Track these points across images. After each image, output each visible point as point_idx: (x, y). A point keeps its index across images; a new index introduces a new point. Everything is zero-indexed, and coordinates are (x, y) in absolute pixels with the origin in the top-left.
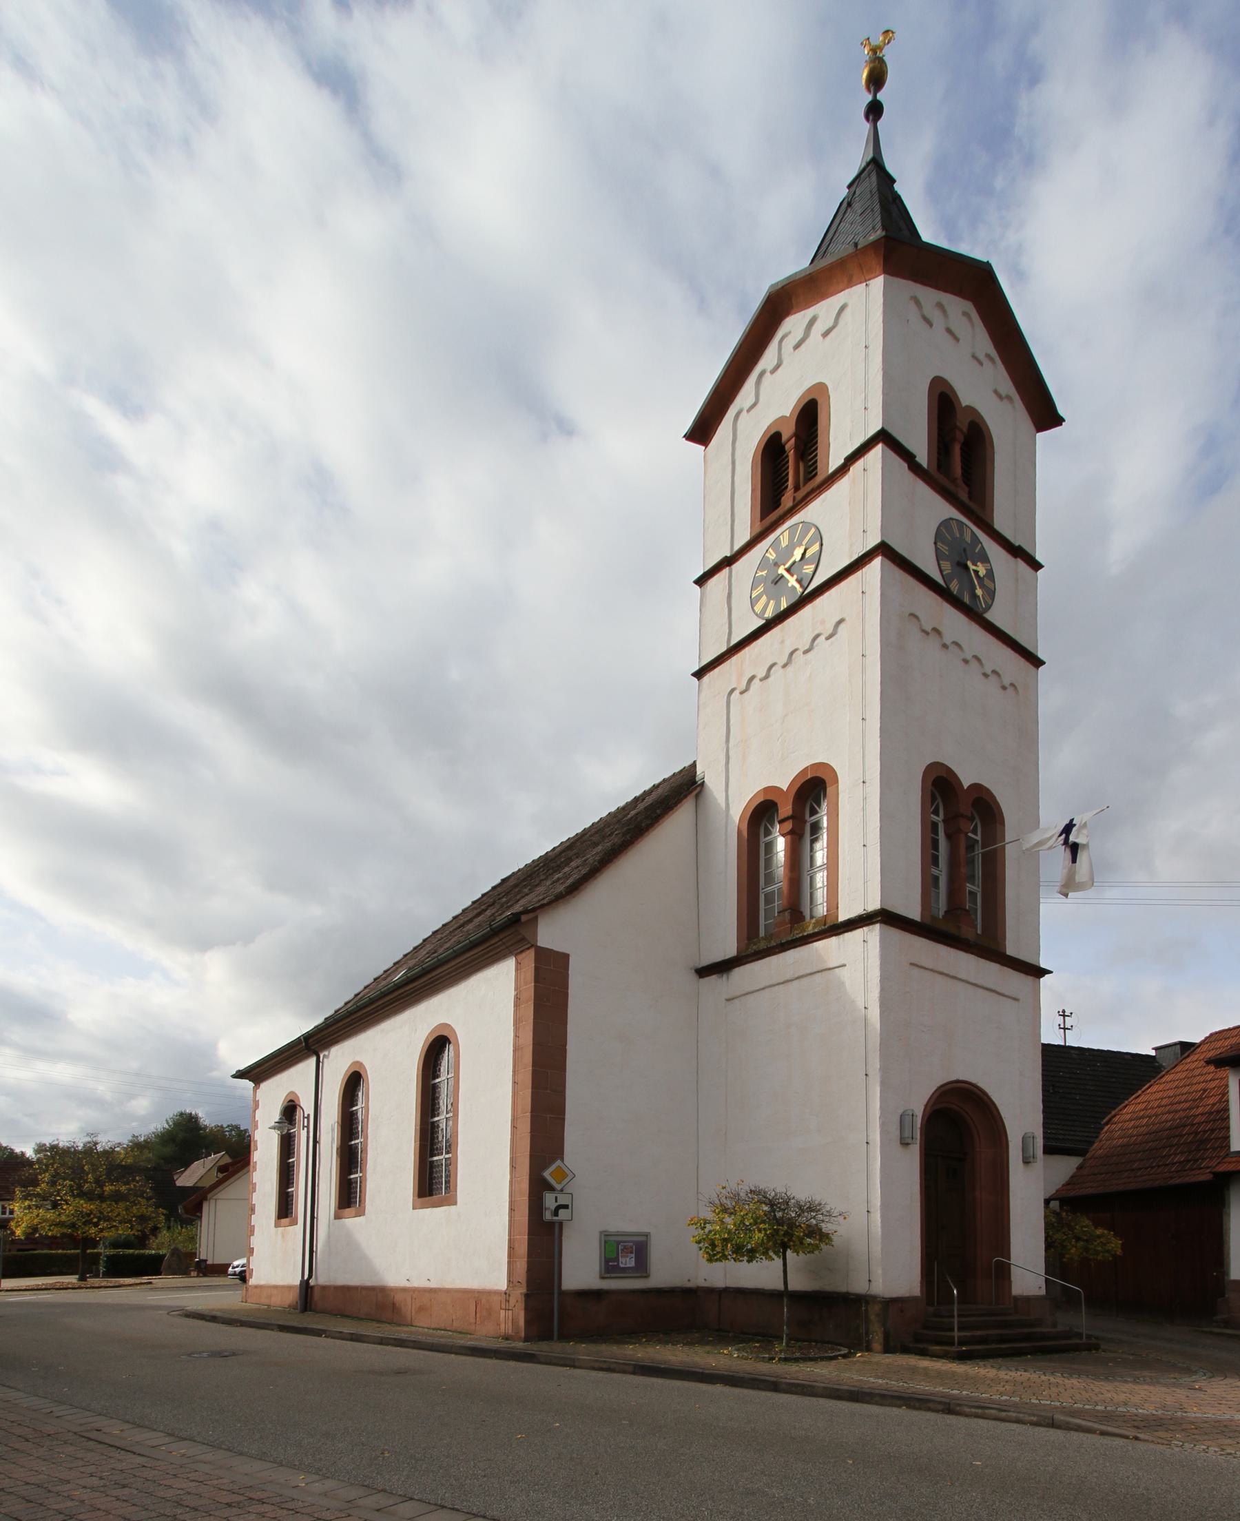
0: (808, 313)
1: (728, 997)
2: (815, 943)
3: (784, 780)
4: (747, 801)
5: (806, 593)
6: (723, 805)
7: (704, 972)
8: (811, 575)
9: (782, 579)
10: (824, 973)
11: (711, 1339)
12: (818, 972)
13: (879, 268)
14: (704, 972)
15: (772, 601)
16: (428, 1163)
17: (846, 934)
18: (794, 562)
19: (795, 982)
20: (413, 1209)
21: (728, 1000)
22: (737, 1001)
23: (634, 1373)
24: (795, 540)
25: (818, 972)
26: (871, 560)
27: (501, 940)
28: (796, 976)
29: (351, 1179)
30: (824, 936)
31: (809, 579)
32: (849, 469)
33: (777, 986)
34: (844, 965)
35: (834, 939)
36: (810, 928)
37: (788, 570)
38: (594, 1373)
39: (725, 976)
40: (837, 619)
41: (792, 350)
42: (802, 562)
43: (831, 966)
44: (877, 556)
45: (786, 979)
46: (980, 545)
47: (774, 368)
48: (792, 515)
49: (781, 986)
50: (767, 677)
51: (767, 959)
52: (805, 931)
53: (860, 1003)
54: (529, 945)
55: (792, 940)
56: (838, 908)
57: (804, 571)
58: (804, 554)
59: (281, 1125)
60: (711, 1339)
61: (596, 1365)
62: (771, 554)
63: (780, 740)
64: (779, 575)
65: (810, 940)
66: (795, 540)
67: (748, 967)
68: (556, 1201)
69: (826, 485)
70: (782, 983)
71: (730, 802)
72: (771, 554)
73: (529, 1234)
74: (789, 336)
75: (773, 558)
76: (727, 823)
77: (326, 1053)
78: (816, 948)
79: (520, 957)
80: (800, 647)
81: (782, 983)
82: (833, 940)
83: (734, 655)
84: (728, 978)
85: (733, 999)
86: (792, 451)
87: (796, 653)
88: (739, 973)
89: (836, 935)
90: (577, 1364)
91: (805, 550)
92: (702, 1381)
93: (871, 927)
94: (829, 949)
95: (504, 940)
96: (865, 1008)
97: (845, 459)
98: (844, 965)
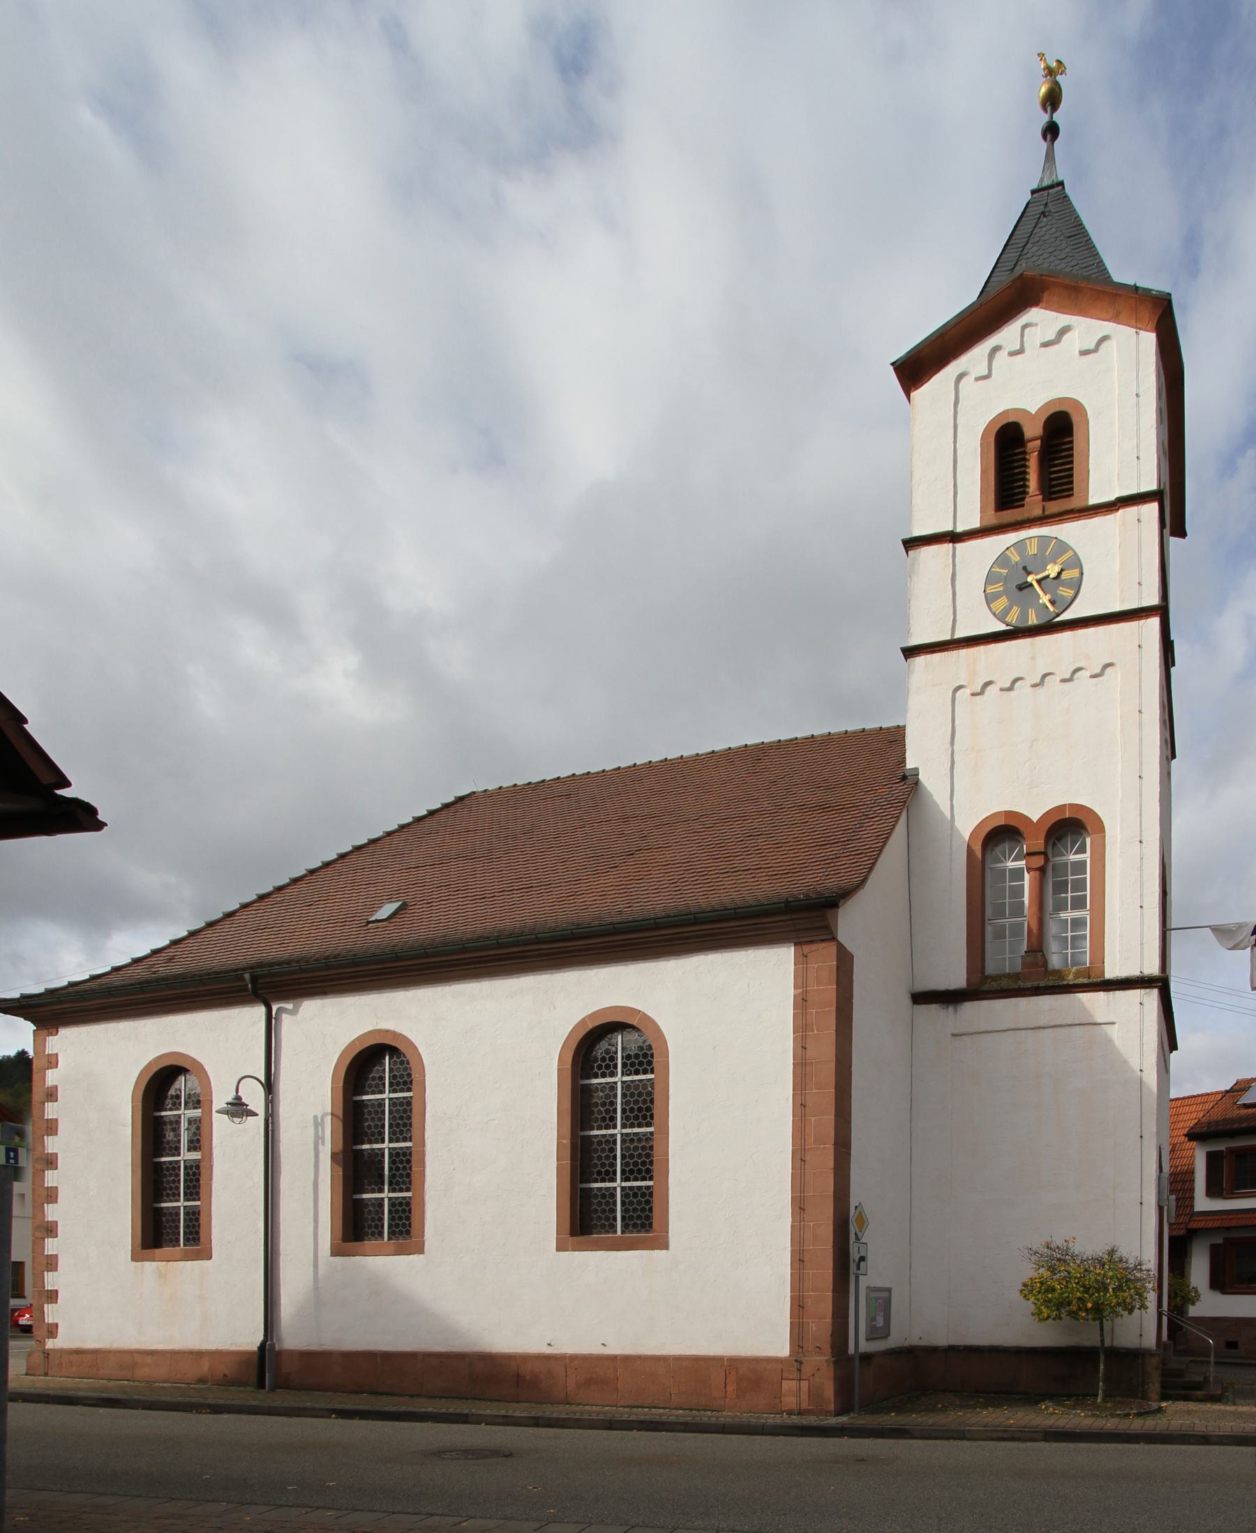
0: (1064, 319)
1: (955, 1032)
2: (1077, 994)
3: (1034, 810)
4: (981, 820)
5: (1058, 619)
6: (949, 816)
7: (920, 998)
8: (1070, 601)
9: (1030, 588)
10: (1086, 1027)
11: (961, 1414)
12: (1080, 1025)
13: (1153, 325)
14: (920, 998)
15: (1015, 608)
16: (579, 1190)
17: (1117, 992)
18: (1048, 576)
19: (1049, 1030)
20: (558, 1249)
21: (954, 1035)
22: (965, 1038)
23: (1046, 1440)
24: (1047, 553)
25: (1080, 1025)
26: (1147, 617)
27: (792, 920)
28: (1052, 1024)
29: (162, 1208)
30: (1091, 989)
31: (1067, 605)
32: (1118, 509)
33: (1024, 1031)
34: (1113, 1023)
35: (1101, 994)
36: (1071, 977)
37: (1039, 582)
38: (1003, 1444)
39: (951, 1009)
40: (1107, 661)
41: (1038, 345)
42: (1056, 581)
43: (1099, 1021)
44: (1155, 615)
45: (1039, 1025)
46: (993, 570)
47: (1015, 351)
48: (1042, 525)
49: (1030, 1032)
50: (1011, 689)
51: (1013, 1000)
52: (1064, 979)
53: (1135, 1063)
54: (830, 937)
55: (1052, 986)
56: (1104, 963)
57: (1058, 591)
58: (1059, 574)
59: (235, 1108)
60: (961, 1414)
61: (995, 1435)
62: (1012, 553)
63: (1027, 764)
64: (1027, 582)
65: (1074, 990)
66: (1047, 553)
67: (984, 1004)
68: (859, 1253)
69: (1093, 512)
70: (1032, 1029)
71: (955, 813)
72: (1012, 553)
73: (834, 1291)
74: (1034, 328)
75: (1016, 560)
76: (951, 834)
77: (289, 1006)
78: (1079, 999)
79: (806, 949)
80: (1057, 672)
81: (1032, 1029)
82: (1101, 995)
83: (963, 647)
84: (956, 1011)
85: (962, 1035)
86: (1036, 453)
87: (1050, 676)
88: (969, 1008)
89: (1104, 991)
90: (968, 1436)
91: (1062, 570)
92: (1127, 1442)
93: (1148, 990)
94: (1096, 1003)
95: (795, 922)
96: (1141, 1070)
97: (1117, 498)
98: (1113, 1023)
